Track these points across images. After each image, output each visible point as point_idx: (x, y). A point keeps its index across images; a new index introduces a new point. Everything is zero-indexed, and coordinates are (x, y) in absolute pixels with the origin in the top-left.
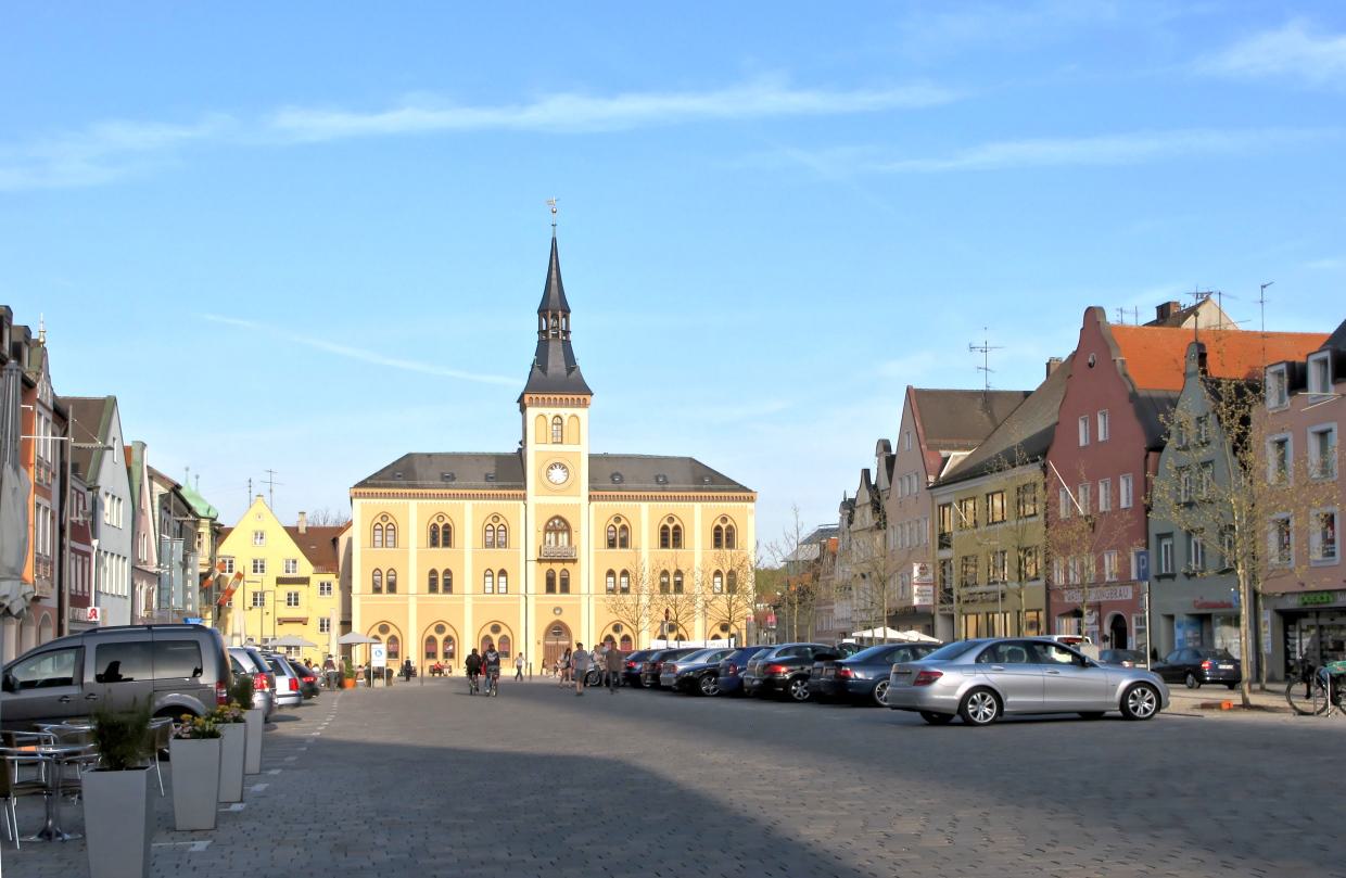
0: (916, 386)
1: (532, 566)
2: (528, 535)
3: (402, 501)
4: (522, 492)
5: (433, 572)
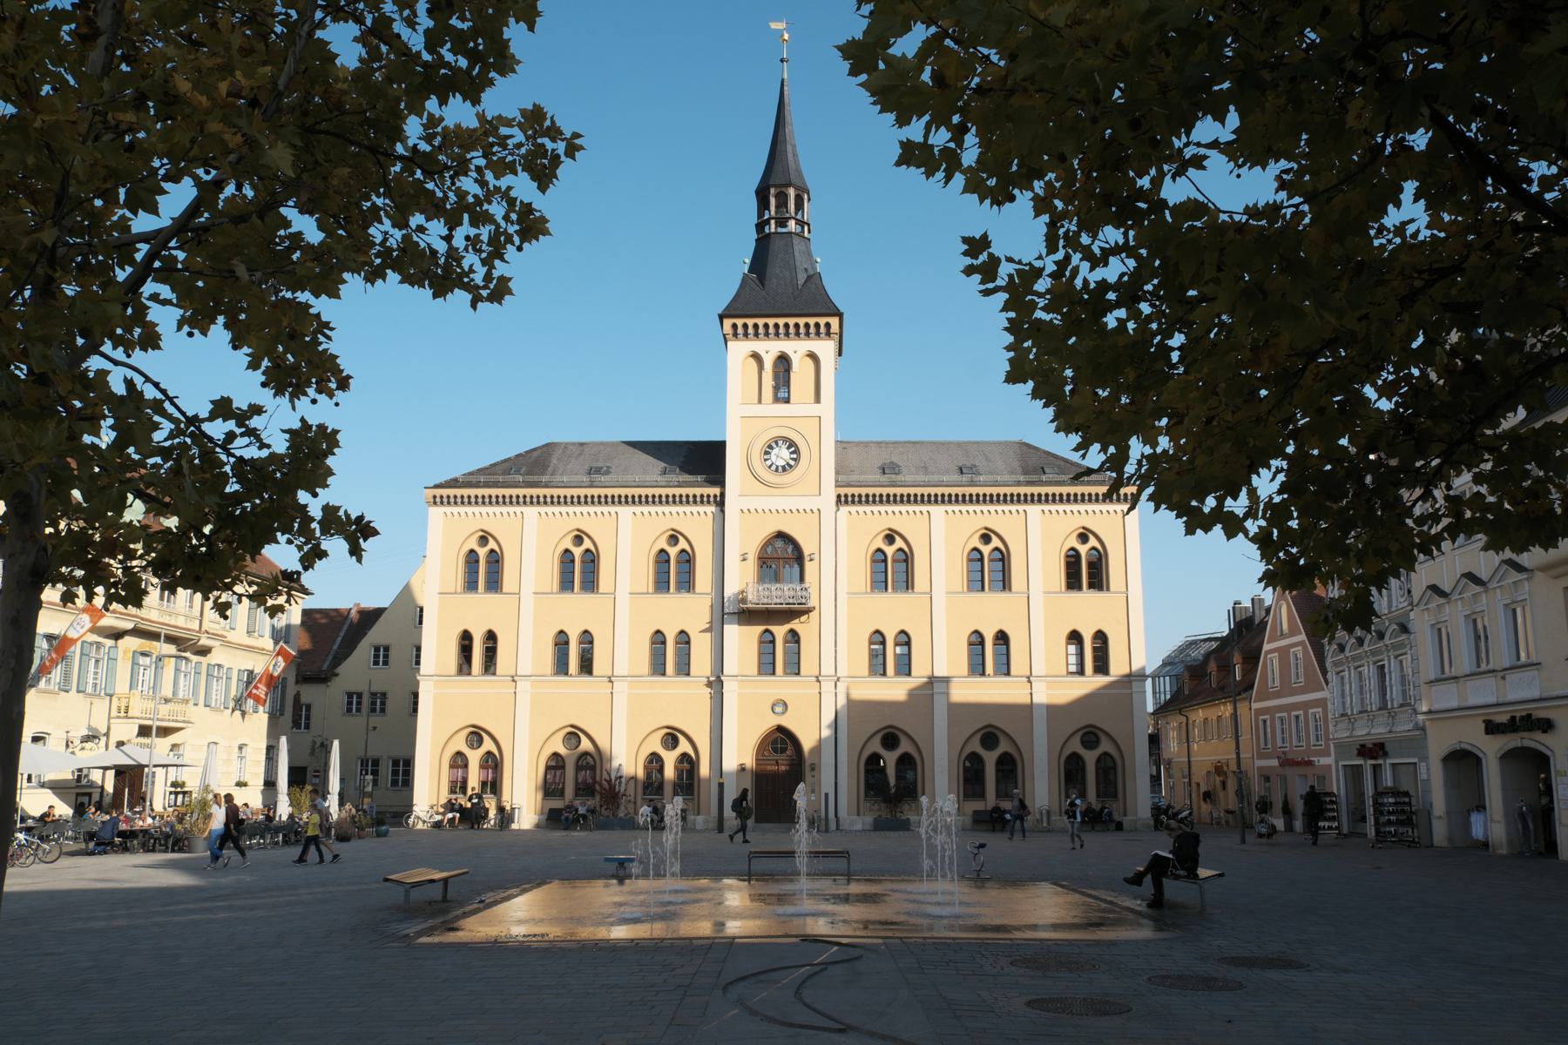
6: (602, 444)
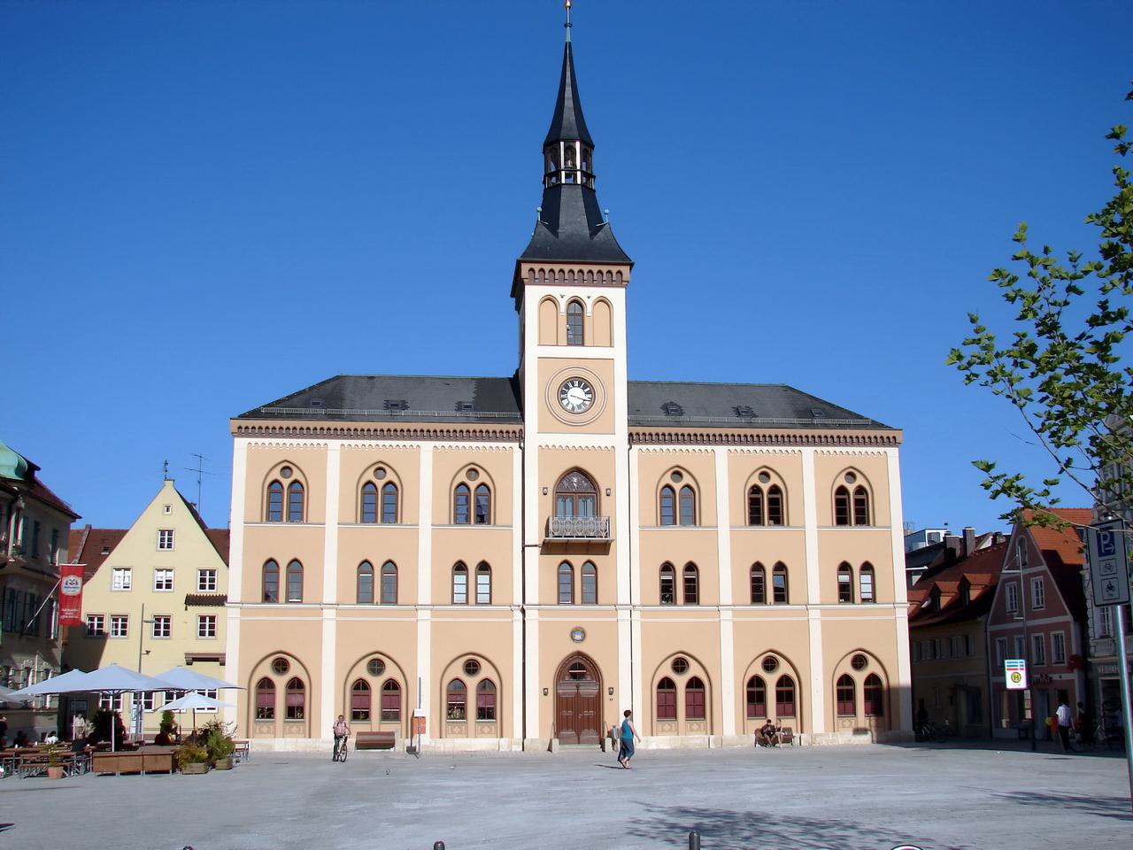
1: (533, 555)
2: (527, 507)
3: (875, 449)
4: (516, 427)
5: (758, 567)
6: (391, 378)
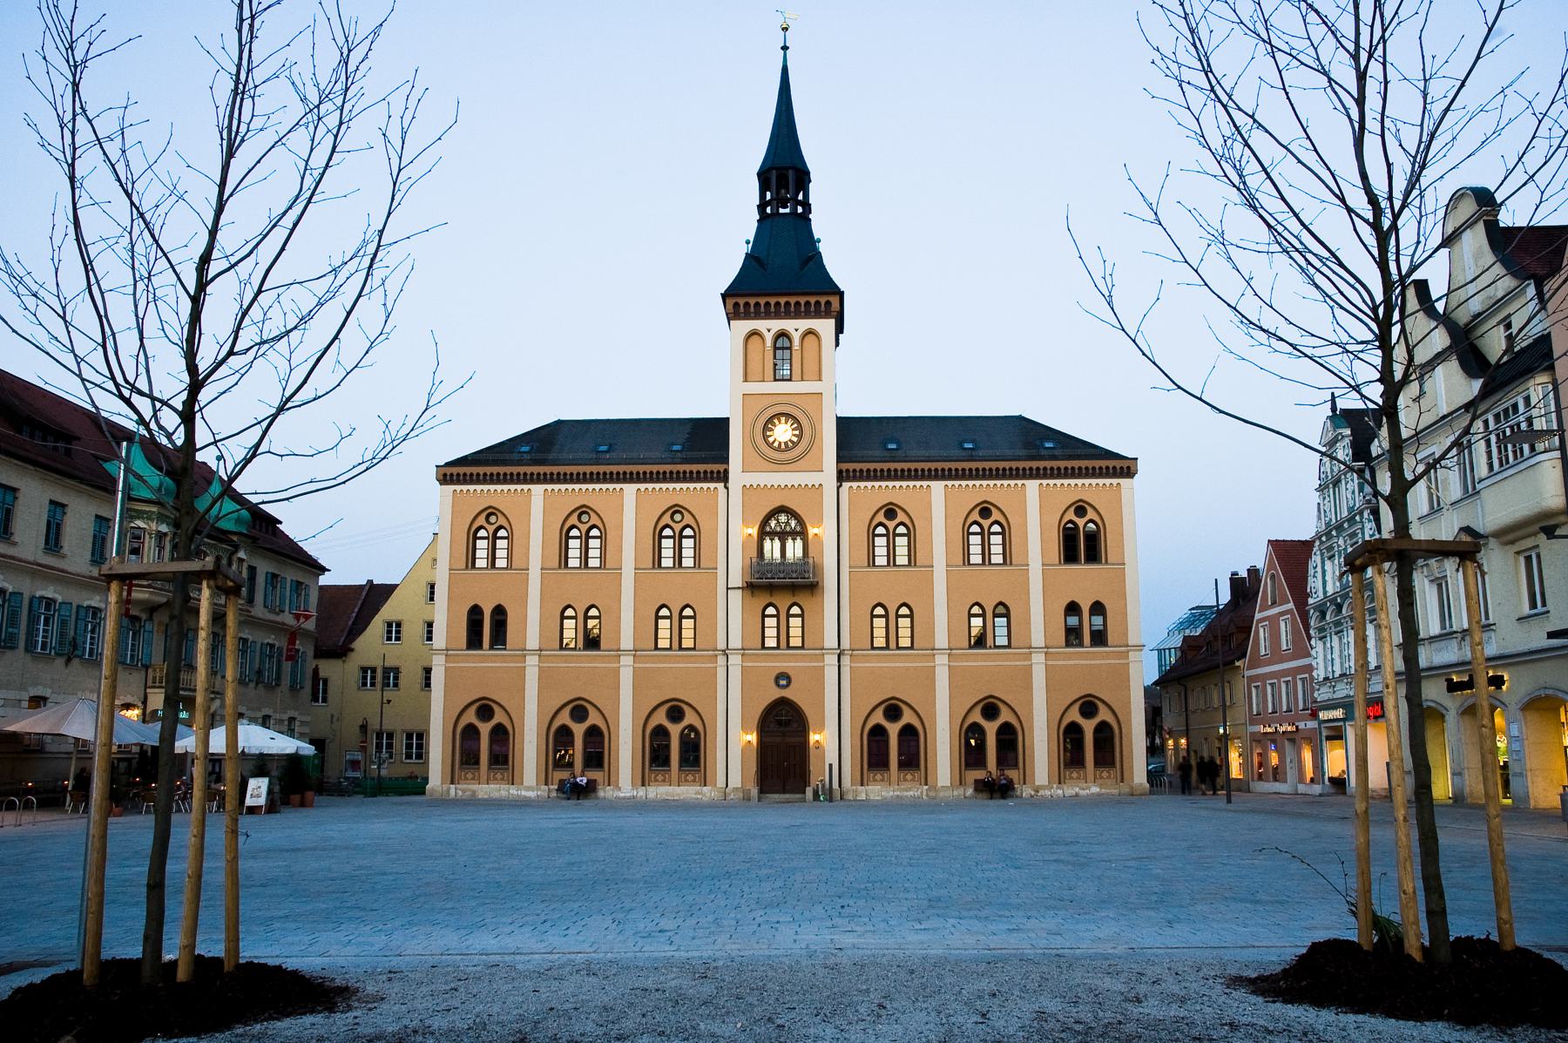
0: (729, 268)
1: (736, 598)
4: (721, 468)
